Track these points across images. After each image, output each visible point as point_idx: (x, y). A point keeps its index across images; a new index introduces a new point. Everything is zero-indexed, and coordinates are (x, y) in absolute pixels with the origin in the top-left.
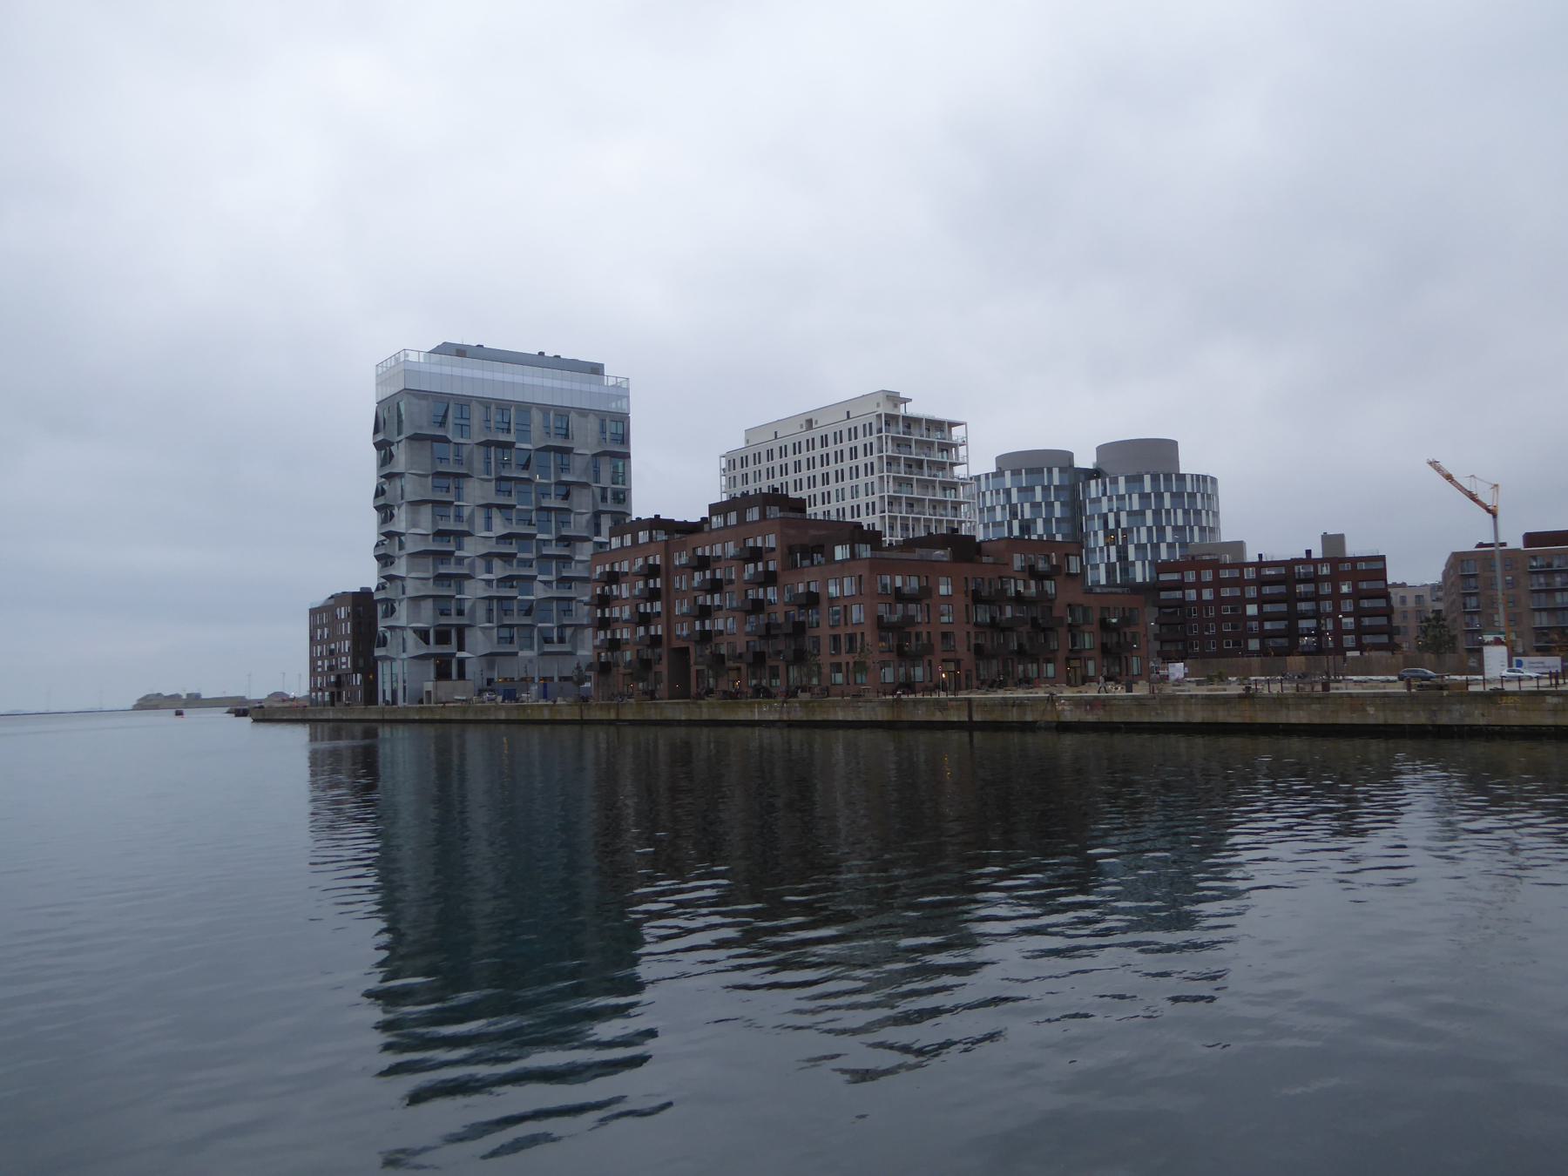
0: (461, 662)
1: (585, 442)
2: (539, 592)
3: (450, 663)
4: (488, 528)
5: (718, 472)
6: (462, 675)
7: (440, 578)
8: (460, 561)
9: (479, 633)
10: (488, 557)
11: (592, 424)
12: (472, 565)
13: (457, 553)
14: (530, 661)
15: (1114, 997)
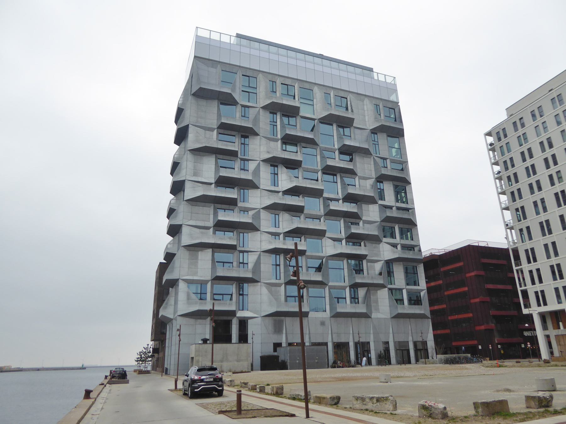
0: (243, 323)
1: (366, 118)
2: (329, 248)
3: (228, 324)
4: (275, 183)
5: (484, 149)
6: (243, 338)
7: (222, 226)
8: (245, 210)
9: (264, 290)
10: (274, 208)
11: (368, 106)
12: (257, 216)
13: (240, 314)
14: (323, 323)
15: (379, 413)
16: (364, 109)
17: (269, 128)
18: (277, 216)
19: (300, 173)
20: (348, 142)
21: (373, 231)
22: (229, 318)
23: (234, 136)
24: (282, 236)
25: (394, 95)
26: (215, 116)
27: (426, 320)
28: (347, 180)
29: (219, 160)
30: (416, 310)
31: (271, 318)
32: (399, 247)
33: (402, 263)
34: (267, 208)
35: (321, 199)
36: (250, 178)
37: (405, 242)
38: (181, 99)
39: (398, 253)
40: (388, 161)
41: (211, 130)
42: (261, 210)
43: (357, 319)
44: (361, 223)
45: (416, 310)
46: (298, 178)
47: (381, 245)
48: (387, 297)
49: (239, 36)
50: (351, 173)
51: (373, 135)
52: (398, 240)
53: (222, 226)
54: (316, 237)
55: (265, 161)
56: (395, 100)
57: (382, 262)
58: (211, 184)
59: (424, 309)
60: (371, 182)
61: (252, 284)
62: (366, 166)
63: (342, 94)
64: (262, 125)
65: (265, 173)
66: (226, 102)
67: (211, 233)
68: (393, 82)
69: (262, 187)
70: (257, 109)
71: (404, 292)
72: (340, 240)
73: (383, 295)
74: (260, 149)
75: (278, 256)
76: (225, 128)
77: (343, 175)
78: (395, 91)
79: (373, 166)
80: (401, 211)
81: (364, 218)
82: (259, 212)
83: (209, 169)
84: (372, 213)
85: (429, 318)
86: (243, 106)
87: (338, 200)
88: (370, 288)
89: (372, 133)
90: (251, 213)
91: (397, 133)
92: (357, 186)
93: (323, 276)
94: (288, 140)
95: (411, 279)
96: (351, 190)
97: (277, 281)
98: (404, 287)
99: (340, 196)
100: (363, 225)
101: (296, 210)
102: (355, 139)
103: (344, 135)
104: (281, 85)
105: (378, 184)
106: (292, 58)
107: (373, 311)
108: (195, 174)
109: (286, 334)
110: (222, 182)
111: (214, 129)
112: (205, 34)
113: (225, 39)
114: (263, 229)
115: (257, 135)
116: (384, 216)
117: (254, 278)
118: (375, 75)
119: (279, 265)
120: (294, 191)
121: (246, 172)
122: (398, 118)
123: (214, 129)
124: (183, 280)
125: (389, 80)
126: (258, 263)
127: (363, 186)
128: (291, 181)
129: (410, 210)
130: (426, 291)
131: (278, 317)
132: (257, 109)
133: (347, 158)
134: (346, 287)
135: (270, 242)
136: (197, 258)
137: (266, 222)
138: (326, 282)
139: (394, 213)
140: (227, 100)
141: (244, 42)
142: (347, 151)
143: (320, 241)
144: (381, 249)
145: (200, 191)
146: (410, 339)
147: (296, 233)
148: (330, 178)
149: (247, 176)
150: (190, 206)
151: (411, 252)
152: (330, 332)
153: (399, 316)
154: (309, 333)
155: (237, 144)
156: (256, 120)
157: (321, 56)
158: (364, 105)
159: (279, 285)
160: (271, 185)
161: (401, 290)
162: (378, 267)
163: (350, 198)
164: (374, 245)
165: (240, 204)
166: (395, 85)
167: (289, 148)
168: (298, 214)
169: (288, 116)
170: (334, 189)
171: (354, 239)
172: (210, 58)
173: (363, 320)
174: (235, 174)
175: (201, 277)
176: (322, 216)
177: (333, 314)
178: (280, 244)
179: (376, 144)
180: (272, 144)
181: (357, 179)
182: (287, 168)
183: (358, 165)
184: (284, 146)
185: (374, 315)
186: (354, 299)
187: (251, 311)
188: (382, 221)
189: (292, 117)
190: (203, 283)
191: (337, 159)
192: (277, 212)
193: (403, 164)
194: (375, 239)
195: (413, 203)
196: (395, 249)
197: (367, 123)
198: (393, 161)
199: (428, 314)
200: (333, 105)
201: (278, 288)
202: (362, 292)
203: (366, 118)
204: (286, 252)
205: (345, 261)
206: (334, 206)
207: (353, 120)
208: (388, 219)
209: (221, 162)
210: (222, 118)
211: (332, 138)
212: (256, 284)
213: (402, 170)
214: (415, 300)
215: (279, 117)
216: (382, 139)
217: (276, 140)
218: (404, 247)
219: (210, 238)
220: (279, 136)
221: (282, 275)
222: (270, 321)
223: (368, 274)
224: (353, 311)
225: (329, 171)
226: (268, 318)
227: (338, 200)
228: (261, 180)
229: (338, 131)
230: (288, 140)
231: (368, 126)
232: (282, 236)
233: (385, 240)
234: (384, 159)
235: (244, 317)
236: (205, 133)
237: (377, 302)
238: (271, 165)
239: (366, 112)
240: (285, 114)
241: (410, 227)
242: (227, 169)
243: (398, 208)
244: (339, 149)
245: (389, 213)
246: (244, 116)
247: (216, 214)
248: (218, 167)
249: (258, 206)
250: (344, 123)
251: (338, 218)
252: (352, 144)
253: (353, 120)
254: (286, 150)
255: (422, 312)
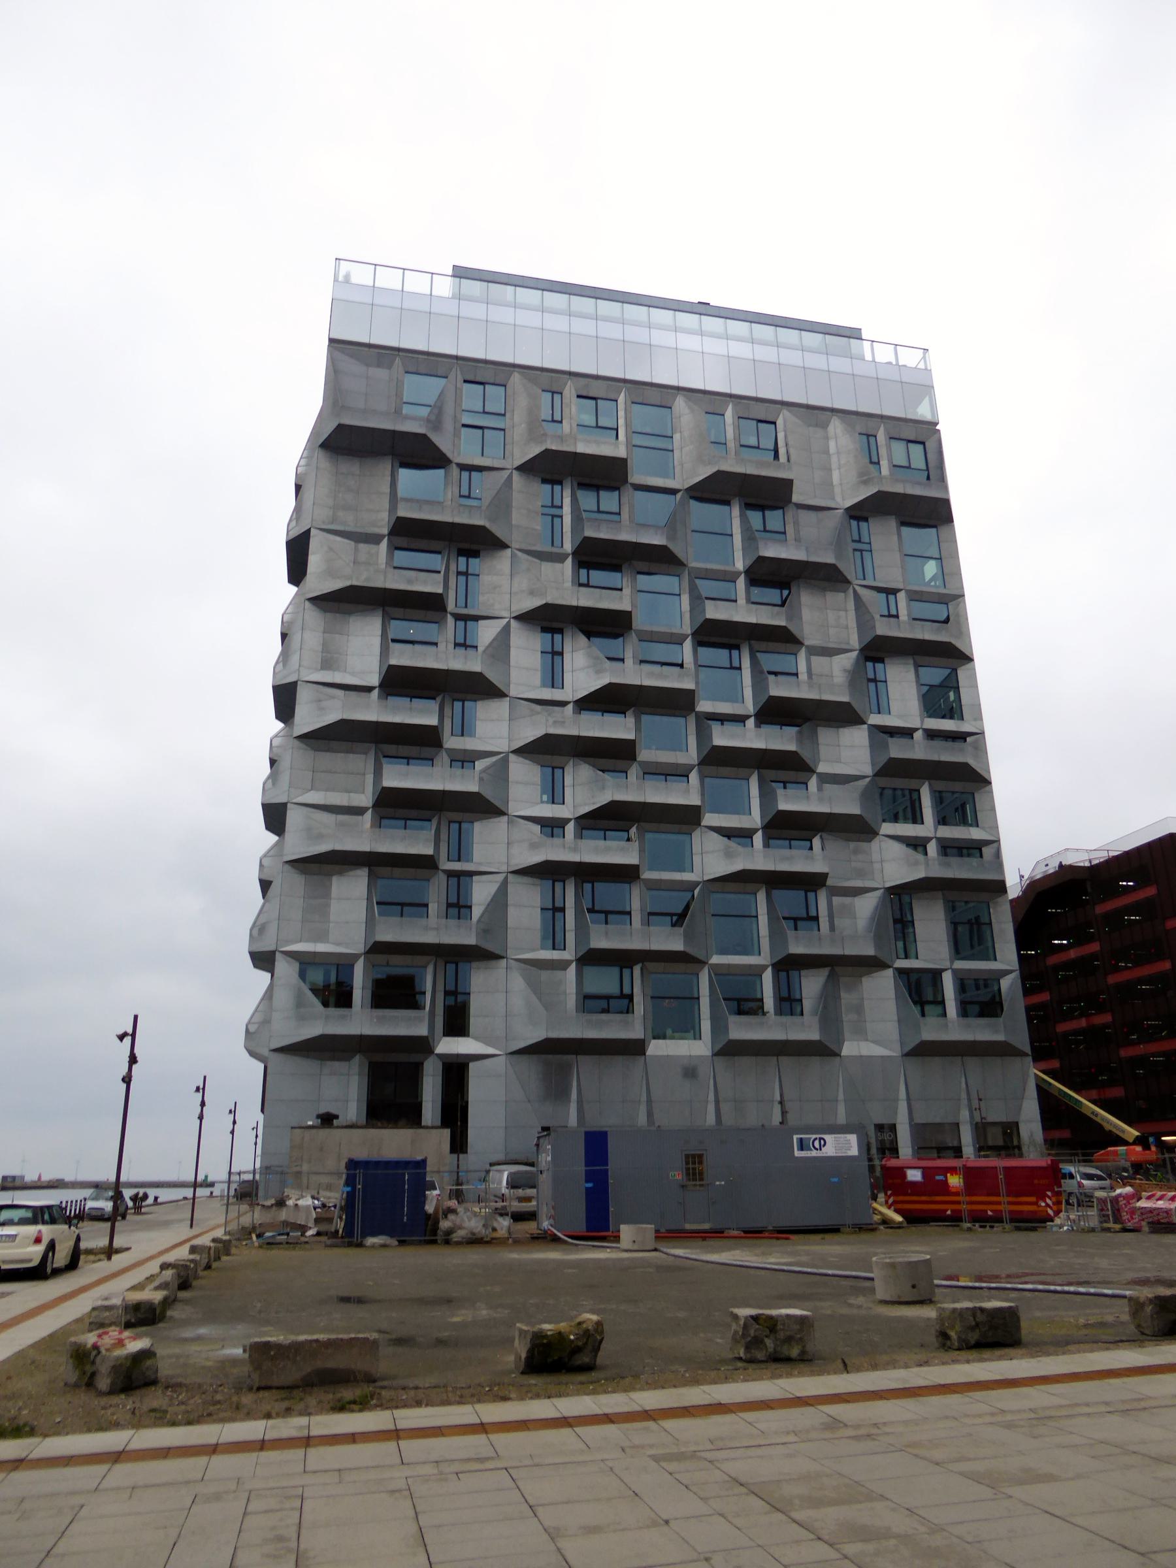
0: (456, 1072)
1: (834, 475)
2: (711, 858)
3: (414, 1074)
4: (554, 678)
7: (394, 805)
8: (465, 759)
9: (518, 982)
10: (549, 751)
11: (840, 441)
14: (690, 1071)
16: (826, 452)
17: (539, 525)
18: (558, 772)
19: (630, 648)
20: (772, 551)
21: (845, 803)
22: (414, 1058)
23: (439, 552)
24: (570, 828)
25: (926, 401)
26: (386, 504)
27: (1018, 1059)
28: (769, 661)
29: (758, 654)
30: (982, 1031)
31: (534, 1057)
32: (932, 848)
33: (940, 894)
34: (529, 750)
35: (692, 720)
36: (477, 668)
37: (947, 832)
38: (303, 462)
39: (931, 866)
40: (901, 596)
41: (374, 539)
42: (512, 757)
43: (754, 1058)
44: (813, 783)
45: (982, 1031)
46: (623, 660)
47: (875, 844)
48: (892, 993)
49: (460, 273)
50: (783, 639)
51: (854, 523)
52: (927, 828)
53: (394, 805)
54: (676, 827)
55: (526, 618)
56: (928, 417)
57: (878, 893)
58: (369, 689)
59: (1010, 1026)
60: (846, 661)
61: (482, 964)
62: (831, 616)
63: (761, 412)
64: (517, 517)
65: (526, 650)
66: (915, 521)
67: (368, 825)
68: (922, 366)
69: (514, 691)
70: (506, 474)
71: (948, 981)
72: (743, 835)
73: (880, 992)
74: (506, 587)
75: (559, 886)
76: (410, 533)
77: (756, 645)
78: (926, 389)
79: (852, 614)
80: (937, 743)
81: (822, 768)
82: (505, 762)
83: (364, 649)
84: (848, 753)
85: (1026, 1055)
86: (463, 467)
87: (741, 719)
88: (837, 969)
89: (852, 517)
90: (480, 765)
91: (930, 513)
92: (803, 676)
93: (688, 938)
94: (595, 556)
95: (970, 935)
96: (779, 689)
97: (556, 955)
98: (947, 964)
99: (749, 706)
100: (820, 789)
101: (612, 755)
102: (798, 540)
103: (765, 531)
104: (574, 399)
105: (870, 665)
106: (607, 319)
107: (847, 1034)
108: (327, 664)
109: (580, 1102)
110: (399, 682)
111: (381, 537)
112: (362, 276)
113: (417, 284)
114: (517, 808)
115: (502, 545)
116: (882, 760)
117: (691, 951)
118: (866, 345)
119: (563, 910)
120: (607, 700)
121: (471, 651)
122: (935, 470)
123: (381, 537)
124: (283, 952)
125: (910, 359)
126: (499, 902)
127: (823, 677)
128: (598, 672)
129: (971, 739)
130: (1015, 975)
131: (553, 1055)
132: (506, 474)
133: (774, 595)
134: (764, 968)
135: (534, 846)
136: (327, 895)
137: (525, 790)
138: (700, 955)
139: (919, 750)
140: (418, 452)
141: (474, 288)
142: (771, 576)
143: (686, 837)
144: (875, 856)
145: (336, 710)
146: (964, 1115)
147: (608, 819)
148: (720, 656)
149: (472, 663)
150: (311, 753)
151: (974, 861)
152: (711, 1097)
153: (923, 1051)
154: (649, 1101)
155: (627, 591)
156: (502, 504)
157: (703, 309)
158: (827, 438)
159: (562, 965)
160: (544, 685)
161: (936, 975)
162: (865, 907)
163: (775, 712)
164: (852, 845)
165: (451, 742)
166: (927, 371)
167: (597, 576)
168: (620, 764)
169: (762, 508)
170: (732, 693)
171: (786, 827)
172: (628, 377)
173: (815, 1064)
174: (442, 657)
175: (338, 944)
176: (691, 768)
177: (718, 1047)
178: (571, 849)
179: (862, 548)
180: (547, 568)
181: (802, 655)
182: (588, 635)
183: (807, 614)
184: (583, 572)
185: (849, 1049)
186: (789, 1003)
187: (476, 1039)
188: (878, 774)
189: (773, 508)
190: (344, 965)
191: (742, 601)
192: (557, 760)
193: (947, 601)
194: (855, 829)
195: (979, 717)
196: (920, 857)
197: (837, 490)
198: (916, 597)
199: (1022, 1040)
200: (731, 445)
201: (559, 974)
202: (811, 985)
203: (834, 475)
204: (774, 881)
205: (761, 896)
206: (722, 737)
207: (788, 484)
208: (892, 769)
209: (398, 628)
210: (587, 524)
211: (732, 538)
212: (493, 963)
213: (947, 621)
214: (981, 1000)
215: (567, 493)
216: (884, 536)
217: (560, 558)
218: (949, 848)
219: (363, 837)
220: (568, 547)
221: (571, 938)
222: (531, 1067)
223: (832, 928)
224: (968, 1036)
225: (713, 635)
226: (525, 1058)
227: (741, 719)
228: (514, 674)
229: (744, 520)
230: (595, 556)
231: (839, 499)
232: (570, 828)
233: (887, 828)
234: (891, 592)
235: (458, 1055)
236: (356, 550)
237: (859, 1009)
238: (544, 630)
239: (834, 459)
240: (587, 481)
241: (969, 786)
242: (418, 647)
243: (931, 735)
244: (748, 572)
245: (897, 750)
246: (469, 497)
247: (378, 773)
248: (388, 642)
249: (503, 746)
250: (765, 495)
251: (743, 771)
252: (783, 555)
253: (788, 484)
254: (587, 585)
255: (1000, 1037)
